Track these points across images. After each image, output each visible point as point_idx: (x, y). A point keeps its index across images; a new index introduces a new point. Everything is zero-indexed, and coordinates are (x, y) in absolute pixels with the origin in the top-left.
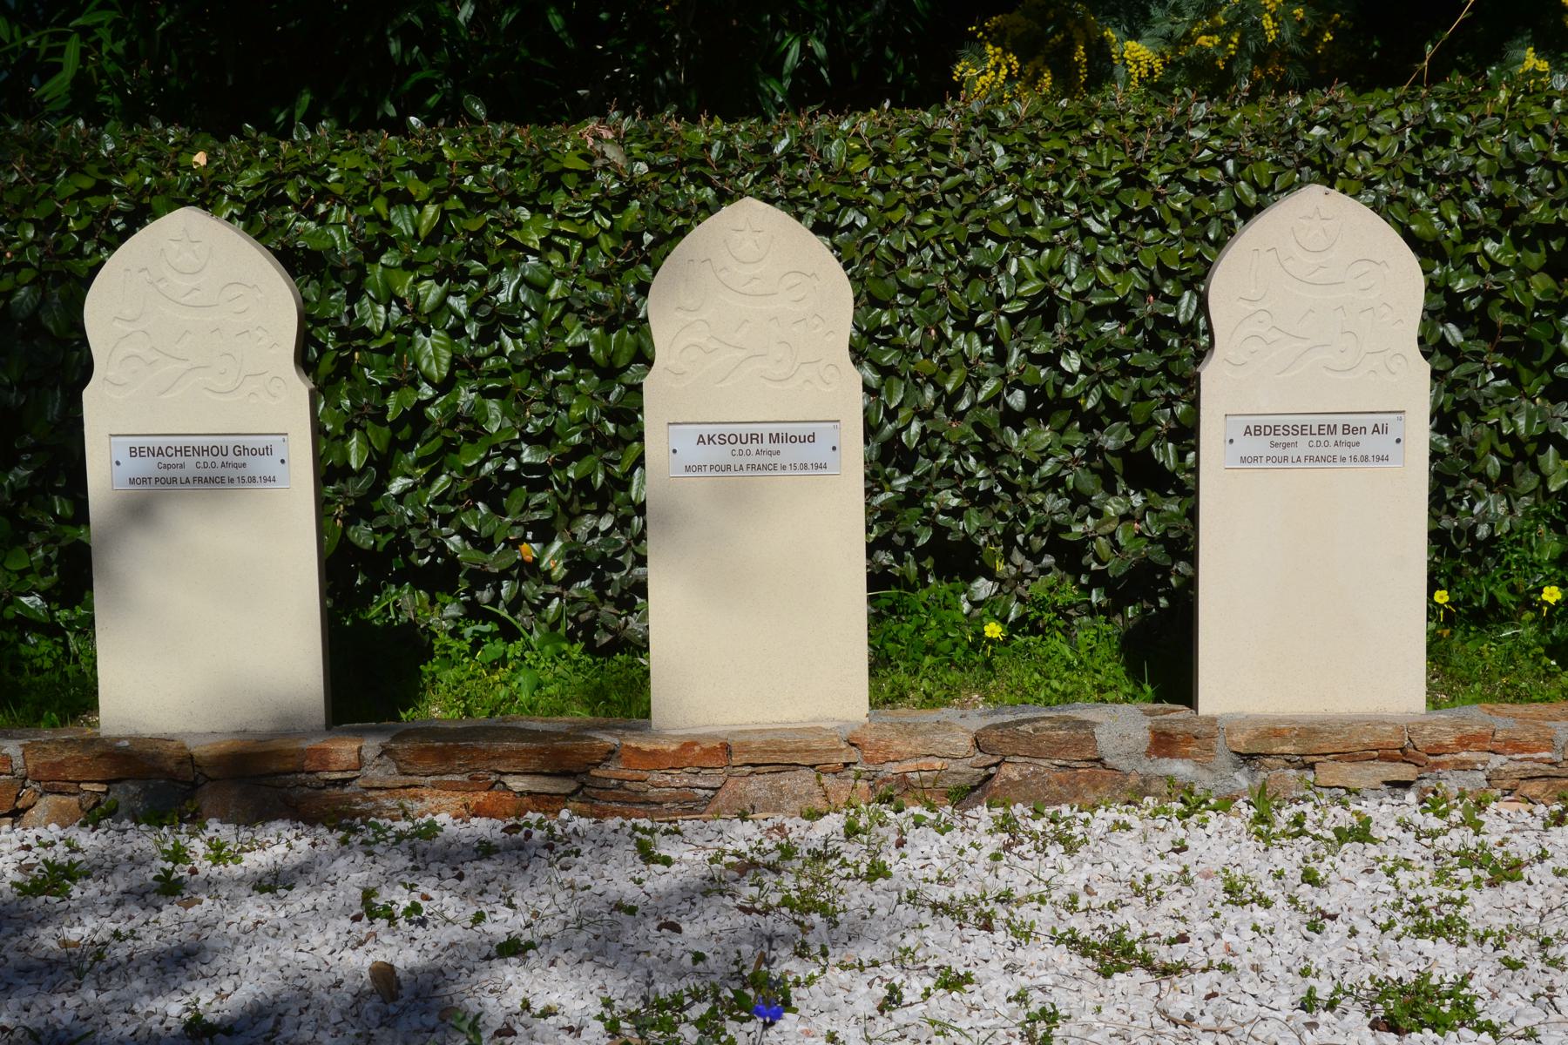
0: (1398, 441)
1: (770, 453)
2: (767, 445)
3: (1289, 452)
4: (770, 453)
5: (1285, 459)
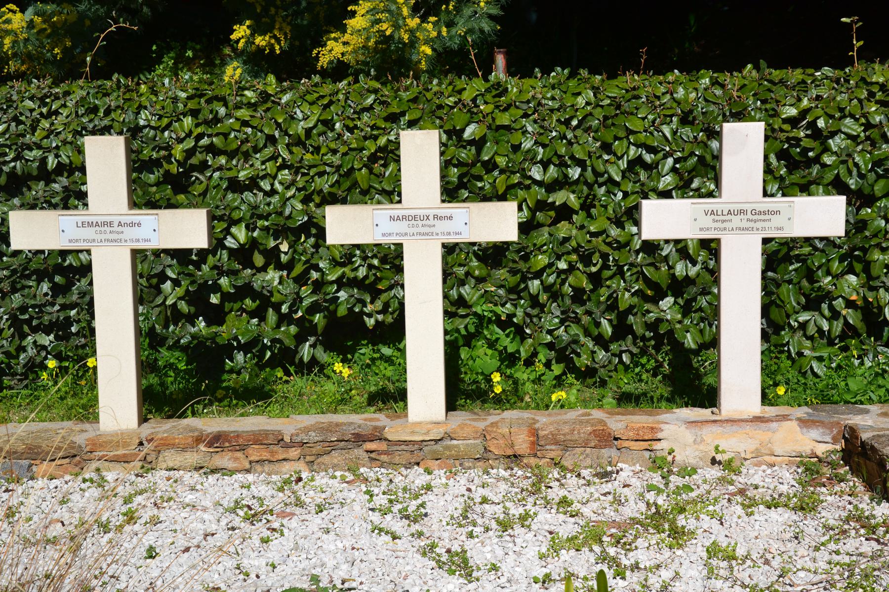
0: (789, 219)
1: (118, 233)
2: (116, 229)
3: (725, 225)
4: (118, 233)
5: (725, 229)
